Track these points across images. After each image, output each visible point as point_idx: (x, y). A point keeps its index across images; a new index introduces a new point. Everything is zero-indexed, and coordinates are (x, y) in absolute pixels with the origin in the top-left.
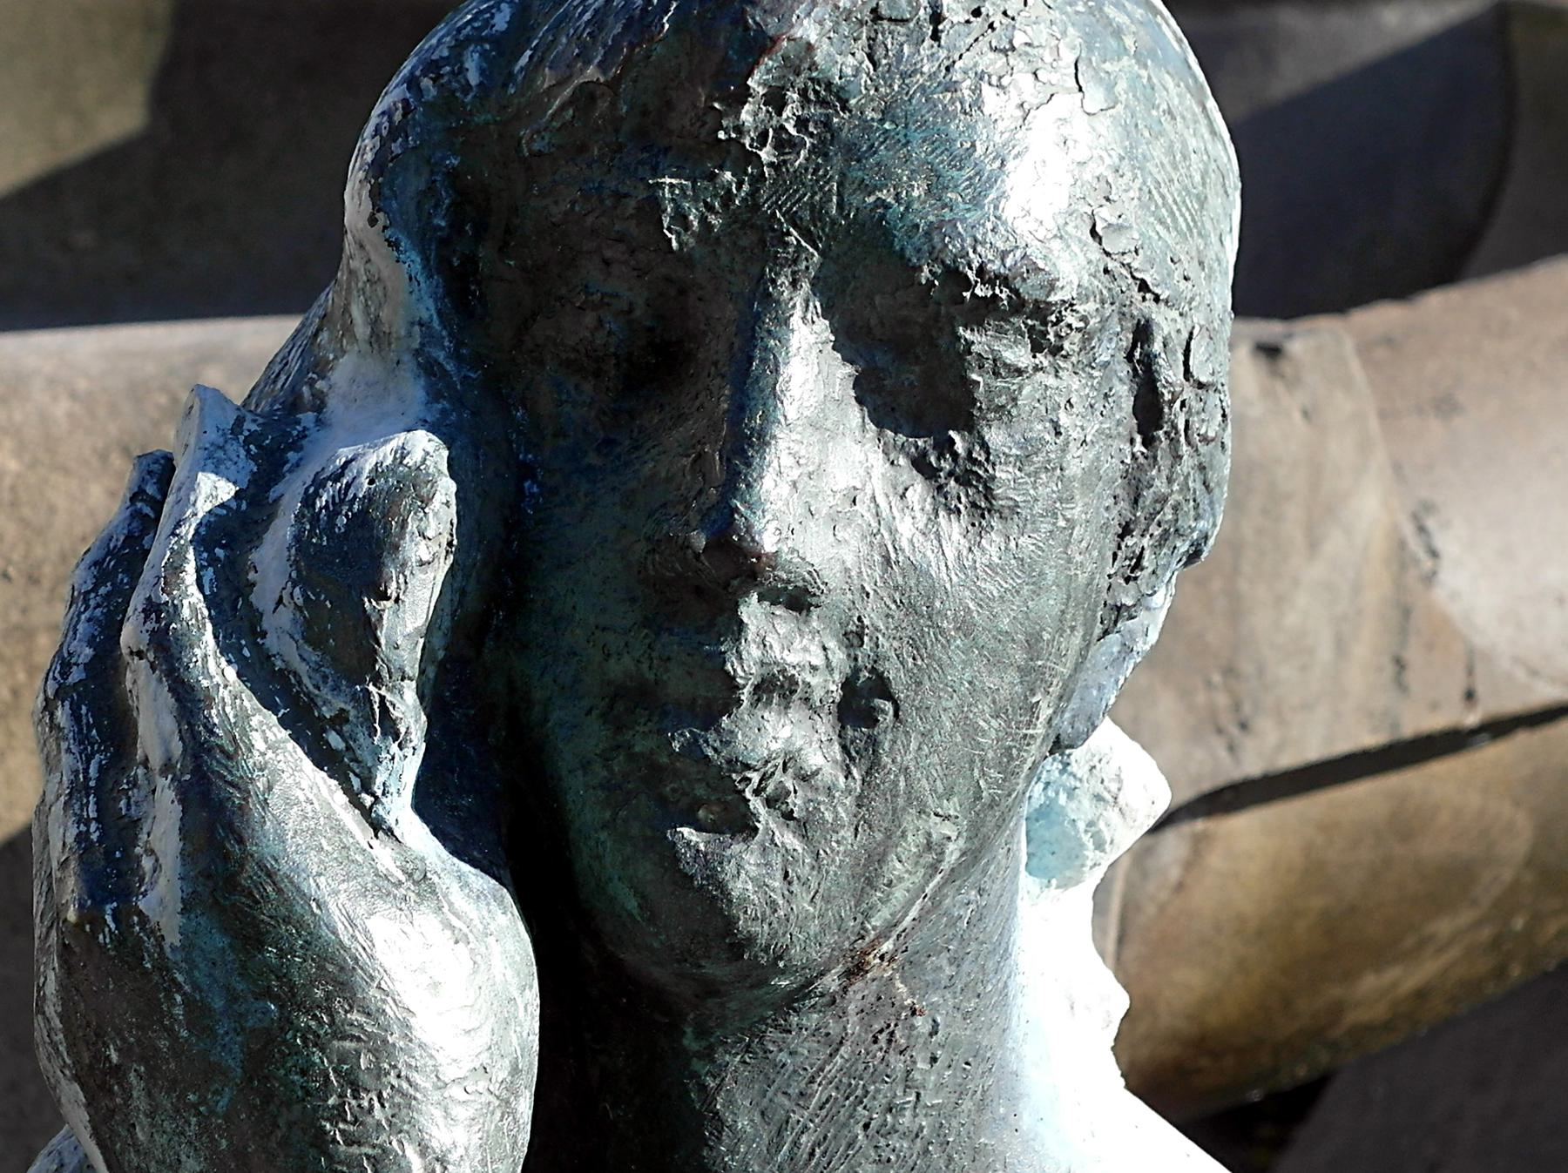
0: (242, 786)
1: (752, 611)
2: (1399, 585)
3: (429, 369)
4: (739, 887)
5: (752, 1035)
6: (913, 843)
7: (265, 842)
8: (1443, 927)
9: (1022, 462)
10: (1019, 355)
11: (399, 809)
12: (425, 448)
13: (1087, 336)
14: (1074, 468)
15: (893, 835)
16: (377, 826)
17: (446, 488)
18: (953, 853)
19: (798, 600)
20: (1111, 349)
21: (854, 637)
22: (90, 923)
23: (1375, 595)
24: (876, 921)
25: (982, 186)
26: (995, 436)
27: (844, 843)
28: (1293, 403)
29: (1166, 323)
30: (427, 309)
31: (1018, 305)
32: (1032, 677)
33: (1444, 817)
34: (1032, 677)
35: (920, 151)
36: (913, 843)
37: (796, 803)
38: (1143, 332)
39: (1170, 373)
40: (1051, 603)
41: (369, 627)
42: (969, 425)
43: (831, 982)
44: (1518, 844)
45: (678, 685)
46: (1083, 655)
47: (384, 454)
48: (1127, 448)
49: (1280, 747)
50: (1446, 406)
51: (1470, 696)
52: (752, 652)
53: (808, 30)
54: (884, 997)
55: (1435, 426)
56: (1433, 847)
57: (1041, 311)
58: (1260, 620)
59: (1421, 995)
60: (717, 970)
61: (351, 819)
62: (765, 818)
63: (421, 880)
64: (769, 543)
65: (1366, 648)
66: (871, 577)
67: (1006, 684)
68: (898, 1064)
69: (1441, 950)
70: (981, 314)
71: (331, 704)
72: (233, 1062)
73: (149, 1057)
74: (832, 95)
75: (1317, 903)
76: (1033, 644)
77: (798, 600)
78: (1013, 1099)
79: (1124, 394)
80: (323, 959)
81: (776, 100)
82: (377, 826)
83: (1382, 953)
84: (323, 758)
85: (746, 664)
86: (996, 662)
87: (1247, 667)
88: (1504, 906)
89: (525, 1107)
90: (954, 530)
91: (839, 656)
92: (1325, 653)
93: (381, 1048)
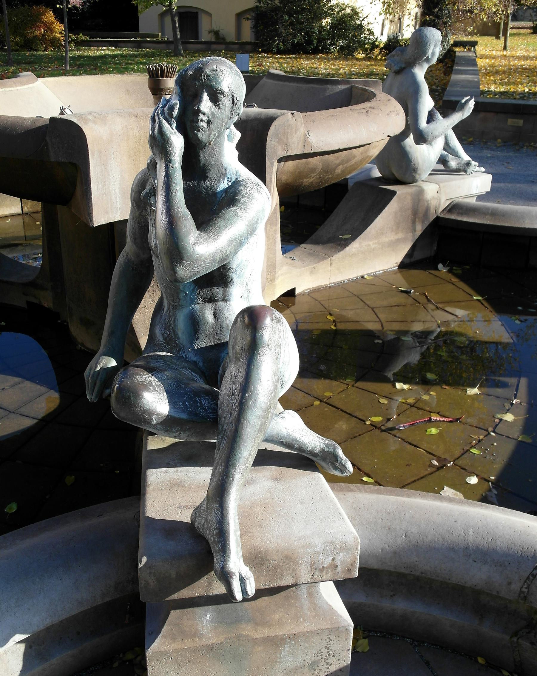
0: (162, 125)
1: (200, 115)
2: (305, 138)
3: (179, 96)
4: (199, 135)
5: (202, 149)
6: (213, 134)
7: (163, 129)
8: (313, 175)
9: (222, 105)
10: (222, 97)
11: (174, 128)
12: (178, 102)
13: (228, 96)
14: (227, 105)
15: (211, 133)
16: (172, 129)
17: (179, 104)
18: (217, 135)
19: (204, 114)
20: (230, 97)
21: (208, 117)
22: (440, 434)
23: (302, 138)
24: (210, 140)
25: (220, 83)
26: (220, 103)
27: (207, 133)
28: (294, 119)
29: (235, 95)
30: (179, 91)
31: (222, 92)
32: (223, 122)
33: (312, 163)
34: (223, 122)
35: (215, 80)
36: (213, 134)
37: (203, 129)
38: (233, 96)
39: (235, 99)
40: (224, 116)
41: (172, 114)
42: (218, 102)
43: (208, 145)
44: (321, 167)
45: (195, 120)
46: (227, 121)
47: (175, 101)
48: (231, 105)
49: (291, 153)
50: (313, 121)
51: (312, 149)
52: (200, 117)
53: (207, 71)
54: (213, 147)
55: (312, 123)
56: (310, 166)
57: (224, 93)
58: (290, 140)
59: (312, 183)
60: (198, 142)
61: (171, 128)
62: (201, 130)
63: (175, 133)
64: (201, 109)
65: (301, 144)
66: (210, 113)
67: (221, 122)
68: (214, 152)
69: (313, 178)
70: (219, 93)
71: (170, 119)
72: (161, 145)
73: (155, 145)
74: (208, 76)
75: (298, 170)
76: (223, 119)
77: (204, 114)
78: (224, 157)
79: (231, 100)
80: (167, 138)
81: (204, 76)
82: (172, 129)
83: (306, 177)
84: (169, 124)
85: (200, 119)
86: (219, 120)
87: (288, 144)
88: (320, 174)
89: (183, 151)
90: (217, 110)
91: (207, 118)
92: (297, 144)
93: (171, 145)
